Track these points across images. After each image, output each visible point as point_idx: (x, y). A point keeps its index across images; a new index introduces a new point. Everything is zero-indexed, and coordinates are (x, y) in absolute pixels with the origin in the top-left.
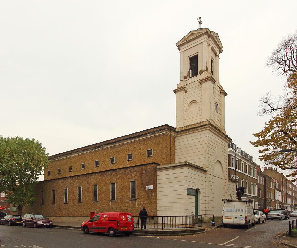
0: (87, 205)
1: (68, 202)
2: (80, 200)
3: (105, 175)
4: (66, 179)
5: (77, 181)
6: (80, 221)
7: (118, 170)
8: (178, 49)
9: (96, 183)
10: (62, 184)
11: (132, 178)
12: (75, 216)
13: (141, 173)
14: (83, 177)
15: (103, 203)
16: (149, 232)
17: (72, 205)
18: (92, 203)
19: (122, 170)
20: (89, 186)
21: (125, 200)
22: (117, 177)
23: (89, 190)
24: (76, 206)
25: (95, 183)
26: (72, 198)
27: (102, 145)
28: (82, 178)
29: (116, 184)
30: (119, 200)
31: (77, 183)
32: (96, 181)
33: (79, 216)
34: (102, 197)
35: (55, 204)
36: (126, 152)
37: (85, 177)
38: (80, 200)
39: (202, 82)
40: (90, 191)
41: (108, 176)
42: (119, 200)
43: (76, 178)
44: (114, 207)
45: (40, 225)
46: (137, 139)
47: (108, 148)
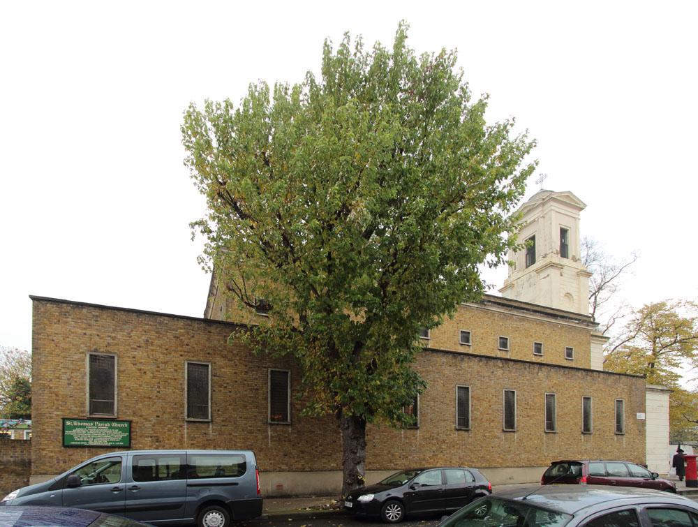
0: (531, 439)
1: (470, 428)
2: (619, 429)
3: (572, 377)
4: (463, 359)
5: (500, 372)
6: (510, 478)
7: (595, 373)
8: (181, 135)
9: (553, 389)
10: (447, 371)
11: (618, 395)
12: (495, 468)
13: (630, 390)
14: (435, 354)
15: (567, 437)
16: (163, 474)
17: (485, 436)
18: (543, 434)
19: (613, 377)
20: (534, 394)
21: (608, 433)
22: (594, 388)
23: (535, 404)
24: (498, 438)
25: (550, 388)
26: (485, 416)
27: (489, 301)
28: (517, 369)
29: (472, 388)
30: (598, 433)
31: (546, 381)
32: (551, 386)
33: (508, 467)
34: (565, 422)
35: (417, 429)
36: (531, 336)
37: (525, 369)
38: (619, 429)
39: (538, 271)
40: (537, 405)
41: (578, 381)
42: (598, 433)
43: (499, 363)
44: (589, 446)
45: (626, 513)
46: (553, 320)
47: (493, 313)
